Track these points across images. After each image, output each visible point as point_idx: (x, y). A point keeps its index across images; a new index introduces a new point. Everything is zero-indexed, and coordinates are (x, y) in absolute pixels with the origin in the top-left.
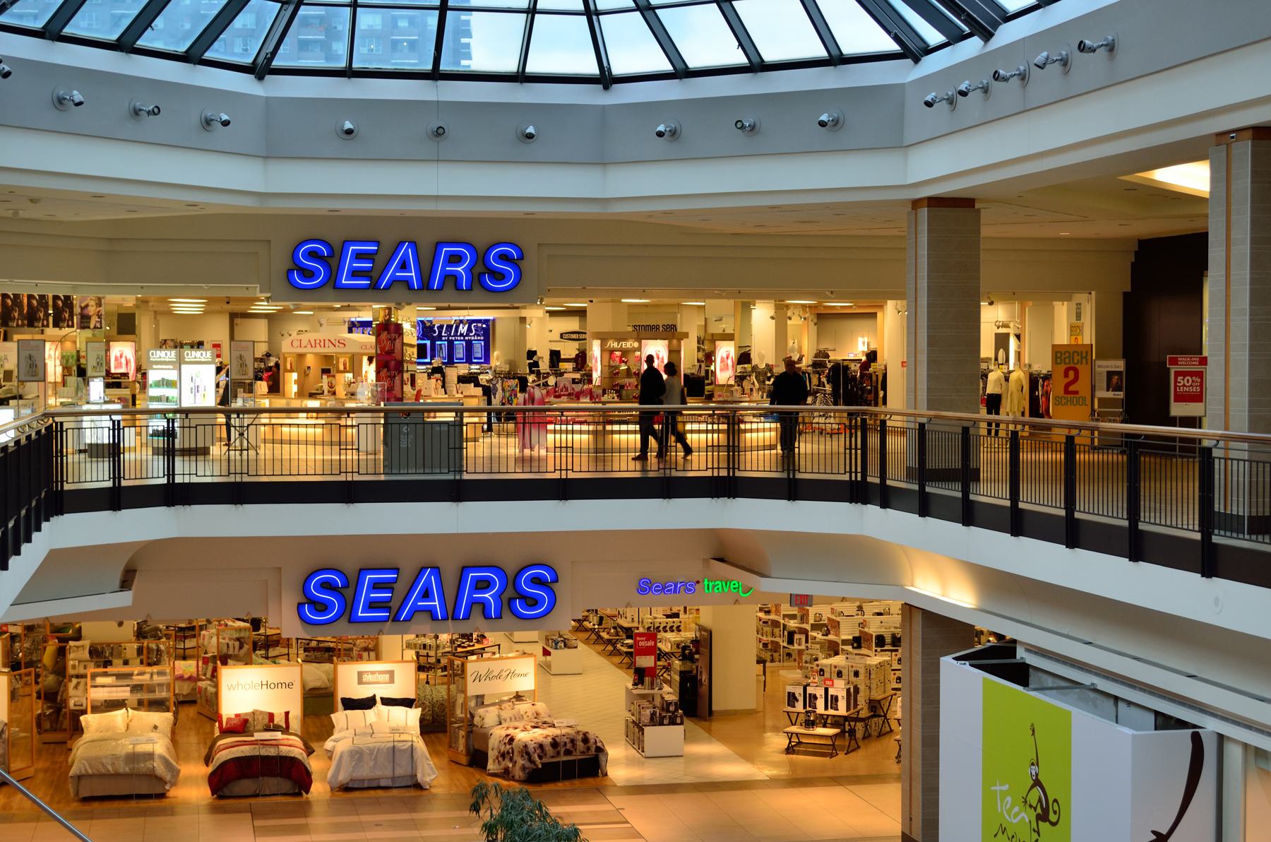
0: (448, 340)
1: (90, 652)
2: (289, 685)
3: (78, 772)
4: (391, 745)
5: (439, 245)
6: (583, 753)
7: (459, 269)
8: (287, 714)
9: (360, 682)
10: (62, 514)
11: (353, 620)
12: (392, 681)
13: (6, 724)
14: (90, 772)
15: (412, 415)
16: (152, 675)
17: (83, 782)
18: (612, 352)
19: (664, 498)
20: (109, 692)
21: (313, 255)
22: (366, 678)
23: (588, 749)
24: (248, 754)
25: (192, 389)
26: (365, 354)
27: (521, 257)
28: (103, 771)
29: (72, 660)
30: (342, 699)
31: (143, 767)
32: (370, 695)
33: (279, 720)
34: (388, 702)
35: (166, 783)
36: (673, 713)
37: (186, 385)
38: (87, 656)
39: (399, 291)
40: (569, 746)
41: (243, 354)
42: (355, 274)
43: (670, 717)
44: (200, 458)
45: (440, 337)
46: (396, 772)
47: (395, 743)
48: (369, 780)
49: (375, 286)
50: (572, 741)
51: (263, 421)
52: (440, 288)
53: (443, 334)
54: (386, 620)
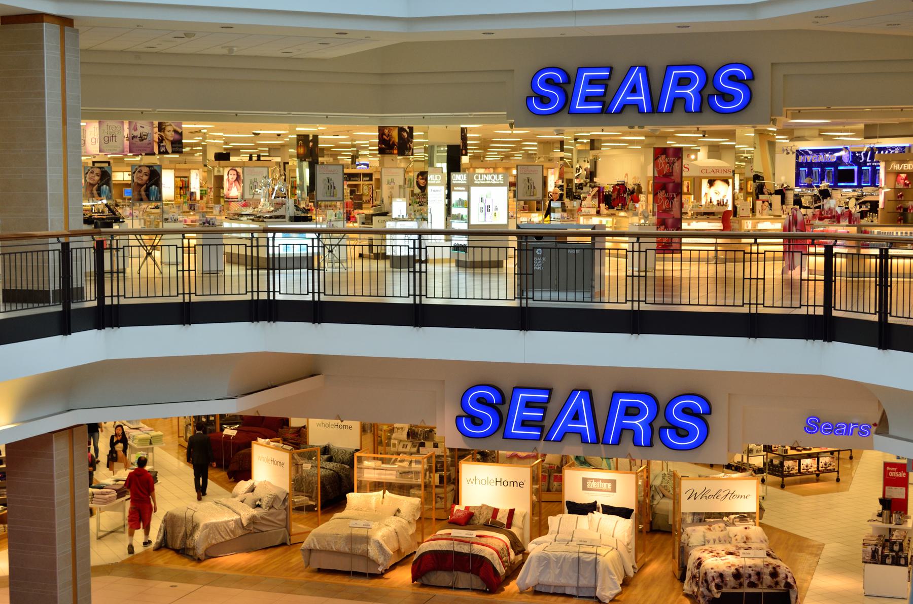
0: (871, 166)
1: (408, 434)
2: (520, 484)
3: (308, 546)
4: (576, 555)
5: (669, 68)
6: (770, 587)
7: (688, 91)
8: (512, 512)
9: (585, 488)
10: (70, 334)
11: (507, 436)
12: (614, 490)
13: (287, 494)
14: (318, 548)
15: (545, 239)
16: (411, 462)
17: (313, 554)
18: (898, 174)
19: (750, 336)
20: (379, 474)
21: (549, 82)
22: (591, 484)
23: (777, 583)
24: (444, 549)
25: (481, 208)
26: (705, 178)
27: (752, 77)
28: (328, 548)
29: (394, 439)
30: (567, 502)
31: (359, 548)
32: (592, 501)
33: (502, 518)
34: (609, 510)
35: (379, 565)
36: (897, 553)
37: (475, 205)
38: (404, 436)
39: (631, 114)
40: (753, 579)
41: (531, 177)
42: (588, 99)
43: (893, 557)
44: (494, 270)
45: (865, 163)
46: (580, 583)
47: (581, 555)
48: (555, 586)
49: (605, 110)
50: (758, 574)
51: (399, 243)
52: (671, 110)
53: (868, 160)
54: (539, 438)
